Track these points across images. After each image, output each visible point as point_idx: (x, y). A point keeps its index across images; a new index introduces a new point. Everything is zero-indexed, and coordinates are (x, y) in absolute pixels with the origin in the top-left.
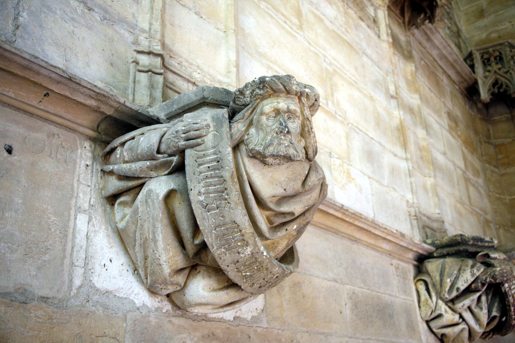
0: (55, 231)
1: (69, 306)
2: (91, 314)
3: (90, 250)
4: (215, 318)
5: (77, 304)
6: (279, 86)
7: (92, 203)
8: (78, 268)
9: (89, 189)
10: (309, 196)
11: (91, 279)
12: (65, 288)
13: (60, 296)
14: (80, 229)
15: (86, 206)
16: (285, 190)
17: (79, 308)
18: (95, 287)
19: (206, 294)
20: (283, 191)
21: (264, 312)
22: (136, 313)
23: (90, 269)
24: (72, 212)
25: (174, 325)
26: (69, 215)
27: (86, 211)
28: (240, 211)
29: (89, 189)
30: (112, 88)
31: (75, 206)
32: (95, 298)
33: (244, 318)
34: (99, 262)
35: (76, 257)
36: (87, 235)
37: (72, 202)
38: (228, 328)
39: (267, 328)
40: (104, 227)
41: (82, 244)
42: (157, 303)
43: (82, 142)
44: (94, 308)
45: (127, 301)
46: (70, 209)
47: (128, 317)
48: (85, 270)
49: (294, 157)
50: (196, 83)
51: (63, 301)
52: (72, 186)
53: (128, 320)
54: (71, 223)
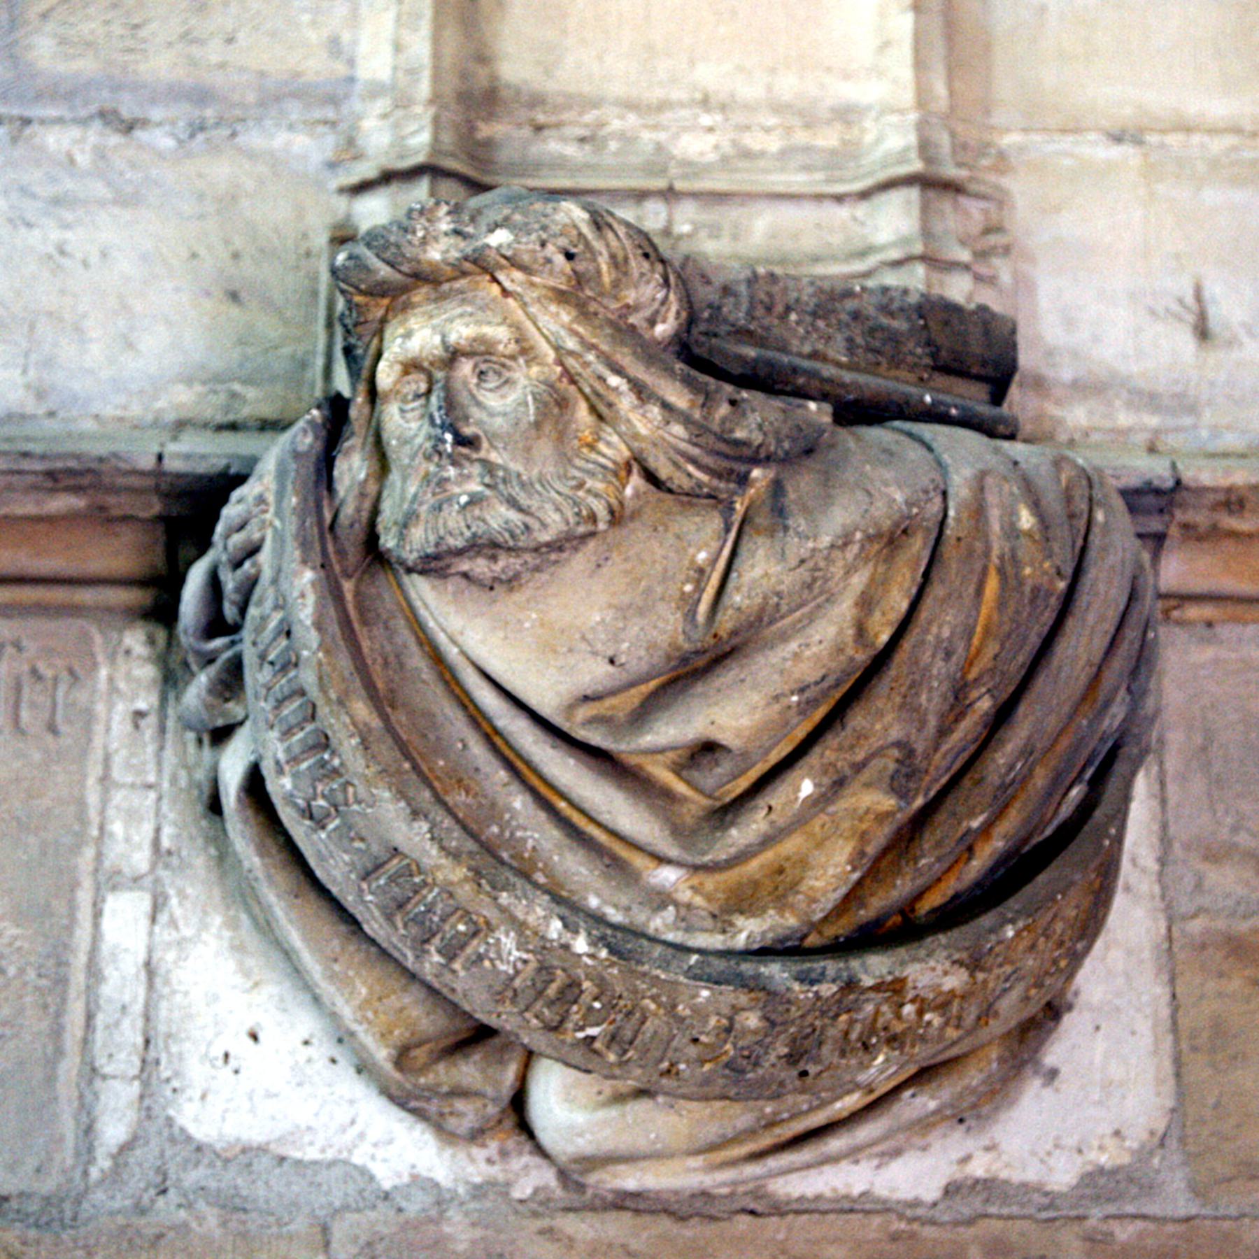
0: (22, 971)
1: (83, 1216)
2: (171, 1234)
3: (163, 1013)
4: (818, 1198)
5: (116, 1205)
6: (376, 272)
7: (166, 843)
8: (116, 1085)
9: (152, 795)
10: (793, 646)
11: (171, 1112)
12: (67, 1155)
13: (48, 1185)
14: (116, 947)
15: (141, 860)
16: (612, 661)
17: (121, 1220)
18: (189, 1139)
19: (580, 1118)
20: (610, 668)
21: (1173, 1143)
22: (372, 1215)
23: (168, 1080)
24: (84, 897)
25: (571, 1242)
26: (72, 907)
27: (141, 877)
28: (391, 807)
29: (152, 795)
30: (237, 387)
31: (96, 870)
32: (192, 1177)
33: (1024, 1185)
34: (203, 1049)
35: (105, 1045)
36: (148, 964)
37: (80, 860)
38: (895, 1237)
39: (1188, 1219)
40: (217, 920)
41: (127, 998)
42: (483, 1166)
43: (115, 635)
44: (182, 1214)
45: (338, 1171)
46: (75, 885)
47: (339, 1232)
48: (146, 1084)
49: (513, 536)
50: (679, 185)
51: (62, 1200)
52: (81, 803)
53: (334, 1245)
54: (83, 935)
